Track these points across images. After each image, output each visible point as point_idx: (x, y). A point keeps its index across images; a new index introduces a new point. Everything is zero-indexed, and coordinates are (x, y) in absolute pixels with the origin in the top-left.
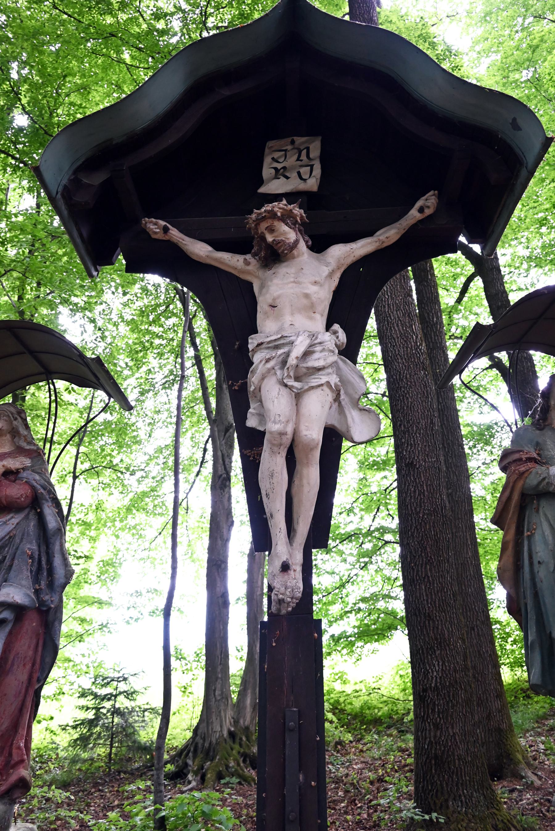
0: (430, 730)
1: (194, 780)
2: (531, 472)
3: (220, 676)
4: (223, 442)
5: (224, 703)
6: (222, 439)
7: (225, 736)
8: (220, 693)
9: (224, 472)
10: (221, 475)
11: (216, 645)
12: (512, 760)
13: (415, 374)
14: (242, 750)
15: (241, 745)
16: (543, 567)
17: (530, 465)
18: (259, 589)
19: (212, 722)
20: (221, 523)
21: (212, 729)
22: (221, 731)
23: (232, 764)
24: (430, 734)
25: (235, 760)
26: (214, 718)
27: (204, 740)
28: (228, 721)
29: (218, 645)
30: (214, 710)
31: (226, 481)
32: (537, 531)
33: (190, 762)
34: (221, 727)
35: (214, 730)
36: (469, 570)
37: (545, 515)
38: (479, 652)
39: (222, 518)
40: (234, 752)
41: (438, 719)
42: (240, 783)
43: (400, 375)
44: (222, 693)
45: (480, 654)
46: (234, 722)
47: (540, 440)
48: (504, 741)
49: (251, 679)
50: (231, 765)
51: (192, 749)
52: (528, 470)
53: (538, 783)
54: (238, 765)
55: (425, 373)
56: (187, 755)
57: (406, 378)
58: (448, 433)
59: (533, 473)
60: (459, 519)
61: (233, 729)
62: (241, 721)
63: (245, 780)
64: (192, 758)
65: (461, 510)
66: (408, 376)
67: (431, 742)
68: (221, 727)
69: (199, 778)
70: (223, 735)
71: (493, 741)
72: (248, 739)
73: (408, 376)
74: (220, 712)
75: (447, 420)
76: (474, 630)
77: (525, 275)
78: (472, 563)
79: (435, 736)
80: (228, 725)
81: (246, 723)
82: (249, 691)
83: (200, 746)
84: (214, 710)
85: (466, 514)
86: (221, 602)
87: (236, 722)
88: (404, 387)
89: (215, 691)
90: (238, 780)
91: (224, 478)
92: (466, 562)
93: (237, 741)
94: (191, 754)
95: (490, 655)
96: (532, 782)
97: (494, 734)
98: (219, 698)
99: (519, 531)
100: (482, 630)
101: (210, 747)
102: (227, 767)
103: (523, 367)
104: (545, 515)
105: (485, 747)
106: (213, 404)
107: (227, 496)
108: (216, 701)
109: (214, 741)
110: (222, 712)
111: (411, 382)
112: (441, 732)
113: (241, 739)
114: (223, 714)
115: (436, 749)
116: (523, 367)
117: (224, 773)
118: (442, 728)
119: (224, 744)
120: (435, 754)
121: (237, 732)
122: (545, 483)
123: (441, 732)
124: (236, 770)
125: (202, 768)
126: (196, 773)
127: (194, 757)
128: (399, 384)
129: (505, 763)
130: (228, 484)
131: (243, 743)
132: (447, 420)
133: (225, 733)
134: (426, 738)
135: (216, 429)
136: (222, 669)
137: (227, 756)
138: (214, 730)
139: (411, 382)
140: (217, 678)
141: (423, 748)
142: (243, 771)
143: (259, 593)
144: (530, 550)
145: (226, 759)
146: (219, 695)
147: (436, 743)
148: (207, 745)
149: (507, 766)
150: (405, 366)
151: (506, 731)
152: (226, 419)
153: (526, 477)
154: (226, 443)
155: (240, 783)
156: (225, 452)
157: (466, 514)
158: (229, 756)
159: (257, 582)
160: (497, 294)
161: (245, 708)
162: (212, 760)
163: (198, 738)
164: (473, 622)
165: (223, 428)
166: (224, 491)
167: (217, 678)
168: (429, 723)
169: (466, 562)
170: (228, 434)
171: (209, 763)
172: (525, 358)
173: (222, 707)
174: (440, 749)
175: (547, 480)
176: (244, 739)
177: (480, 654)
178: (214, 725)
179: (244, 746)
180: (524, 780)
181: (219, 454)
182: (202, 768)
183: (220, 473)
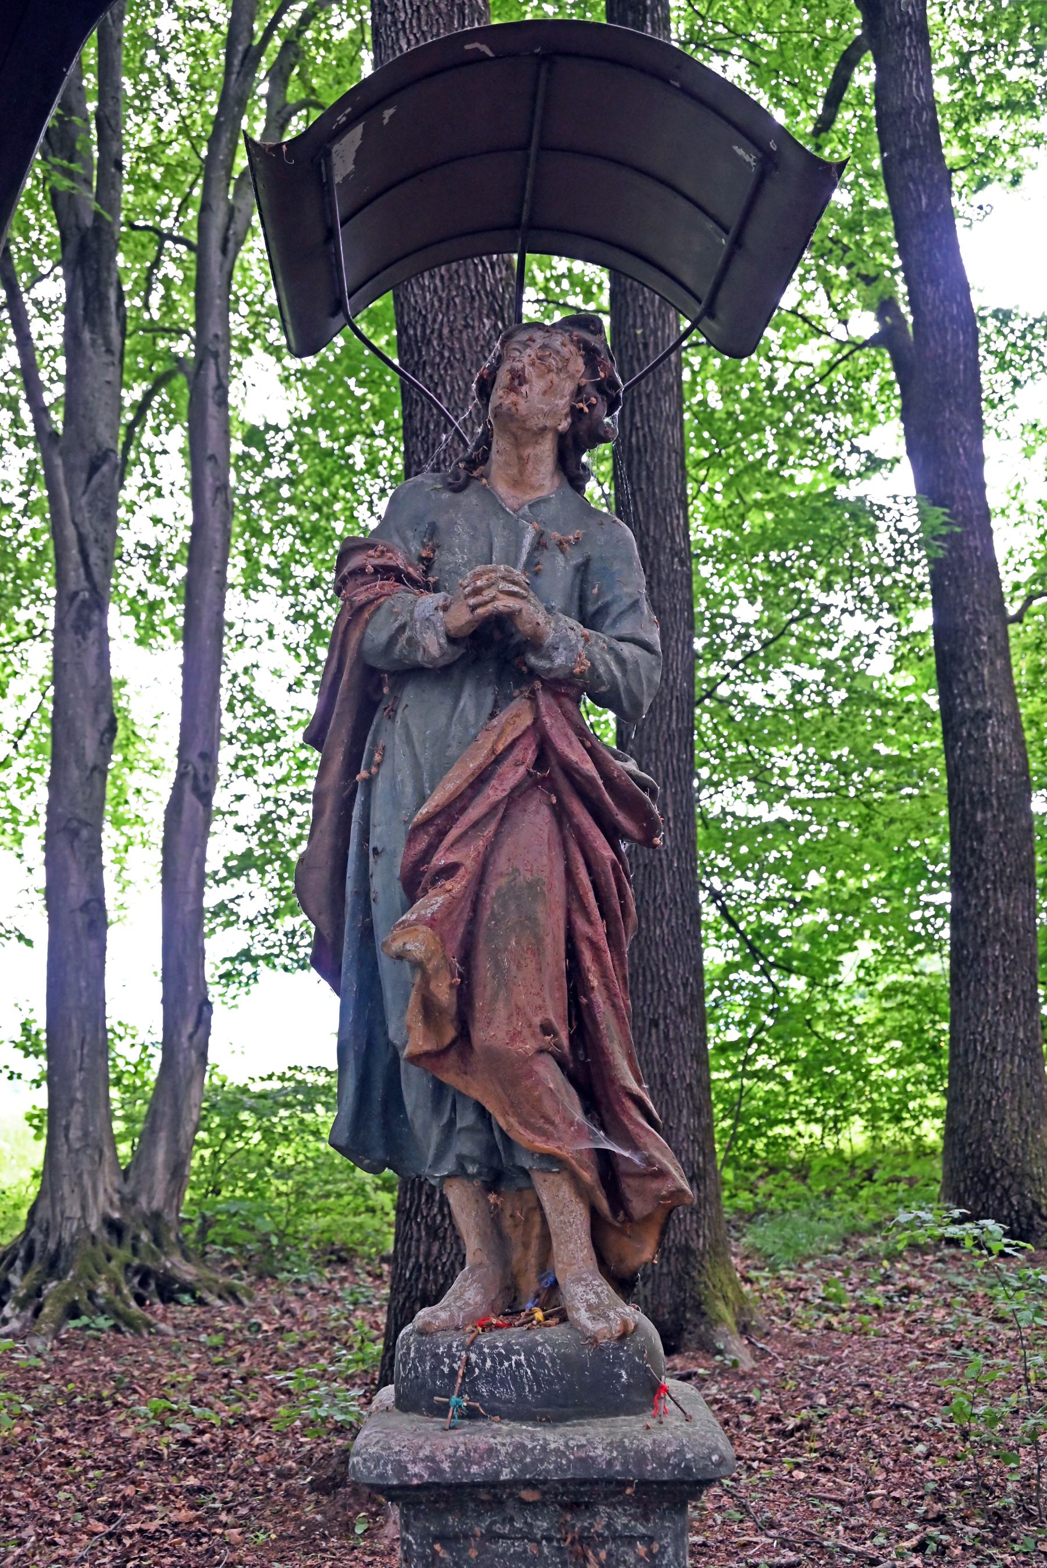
0: (418, 1240)
1: (17, 1317)
2: (378, 608)
3: (79, 1095)
4: (84, 501)
5: (92, 1158)
6: (80, 490)
7: (93, 1228)
8: (79, 1133)
9: (85, 584)
10: (76, 594)
11: (70, 1025)
12: (704, 1314)
13: (467, 326)
14: (136, 1262)
15: (135, 1251)
16: (382, 861)
17: (389, 585)
18: (191, 898)
19: (63, 1198)
20: (78, 724)
21: (62, 1213)
22: (84, 1217)
23: (102, 1288)
24: (418, 1248)
25: (112, 1281)
26: (66, 1189)
27: (47, 1233)
28: (101, 1197)
29: (74, 1023)
30: (65, 1172)
31: (91, 609)
32: (383, 770)
33: (15, 1279)
34: (84, 1208)
35: (67, 1214)
36: (662, 883)
37: (406, 726)
38: (663, 1076)
39: (81, 710)
40: (113, 1264)
41: (439, 1218)
42: (116, 1328)
43: (423, 326)
44: (86, 1134)
45: (664, 1083)
46: (122, 1200)
47: (442, 522)
48: (695, 1274)
49: (167, 1109)
50: (99, 1291)
51: (22, 1253)
52: (370, 602)
53: (747, 1364)
54: (118, 1291)
55: (495, 326)
56: (11, 1264)
57: (440, 336)
58: (647, 516)
59: (383, 612)
60: (649, 751)
61: (116, 1215)
62: (143, 1200)
63: (129, 1324)
64: (19, 1271)
65: (659, 728)
66: (446, 331)
67: (417, 1267)
68: (84, 1208)
69: (29, 1313)
70: (87, 1227)
71: (669, 1273)
72: (157, 1239)
73: (446, 331)
74: (80, 1176)
75: (650, 478)
76: (657, 1025)
77: (1031, 59)
78: (670, 866)
79: (428, 1254)
80: (104, 1203)
81: (156, 1204)
82: (163, 1135)
83: (38, 1247)
84: (65, 1172)
85: (670, 739)
86: (80, 924)
87: (128, 1201)
88: (433, 365)
89: (67, 1128)
90: (111, 1322)
91: (84, 602)
92: (656, 863)
93: (128, 1240)
94: (18, 1264)
95: (690, 1085)
96: (735, 1363)
97: (673, 1259)
98: (77, 1145)
99: (353, 764)
100: (677, 1028)
101: (57, 1251)
102: (92, 1295)
103: (944, 347)
104: (406, 726)
105: (649, 1285)
106: (54, 393)
107: (94, 651)
108: (70, 1150)
109: (67, 1238)
110: (86, 1177)
111: (452, 350)
112: (443, 1246)
113: (136, 1238)
114: (87, 1180)
115: (426, 1281)
116: (944, 347)
117: (82, 1307)
118: (444, 1238)
119: (89, 1245)
120: (424, 1290)
121: (127, 1221)
122: (402, 640)
123: (443, 1246)
124: (109, 1302)
125: (39, 1295)
126: (22, 1304)
127: (25, 1270)
128: (420, 356)
129: (688, 1321)
130: (95, 618)
131: (141, 1245)
132: (650, 478)
133: (94, 1224)
134: (409, 1256)
135: (58, 461)
136: (83, 1083)
137: (93, 1271)
138: (67, 1214)
139: (452, 350)
140: (73, 1101)
141: (402, 1276)
142: (128, 1305)
143: (189, 907)
144: (366, 818)
145: (91, 1278)
146: (79, 1139)
147: (428, 1269)
148: (52, 1246)
149: (690, 1327)
150: (440, 300)
151: (703, 1255)
152: (93, 434)
153: (367, 622)
154: (90, 504)
155: (116, 1328)
156: (87, 529)
157: (670, 739)
158: (99, 1272)
159: (185, 880)
160: (904, 112)
161: (151, 1171)
162: (60, 1279)
163: (34, 1231)
164: (656, 1009)
165: (81, 459)
166: (85, 638)
167: (73, 1101)
168: (418, 1224)
169: (656, 863)
170: (97, 479)
171: (54, 1283)
172: (953, 319)
173: (86, 1166)
174: (435, 1282)
175: (408, 633)
176: (145, 1236)
177: (664, 1083)
178: (67, 1203)
179: (143, 1252)
180: (718, 1358)
181: (70, 532)
182: (39, 1293)
183: (72, 587)
